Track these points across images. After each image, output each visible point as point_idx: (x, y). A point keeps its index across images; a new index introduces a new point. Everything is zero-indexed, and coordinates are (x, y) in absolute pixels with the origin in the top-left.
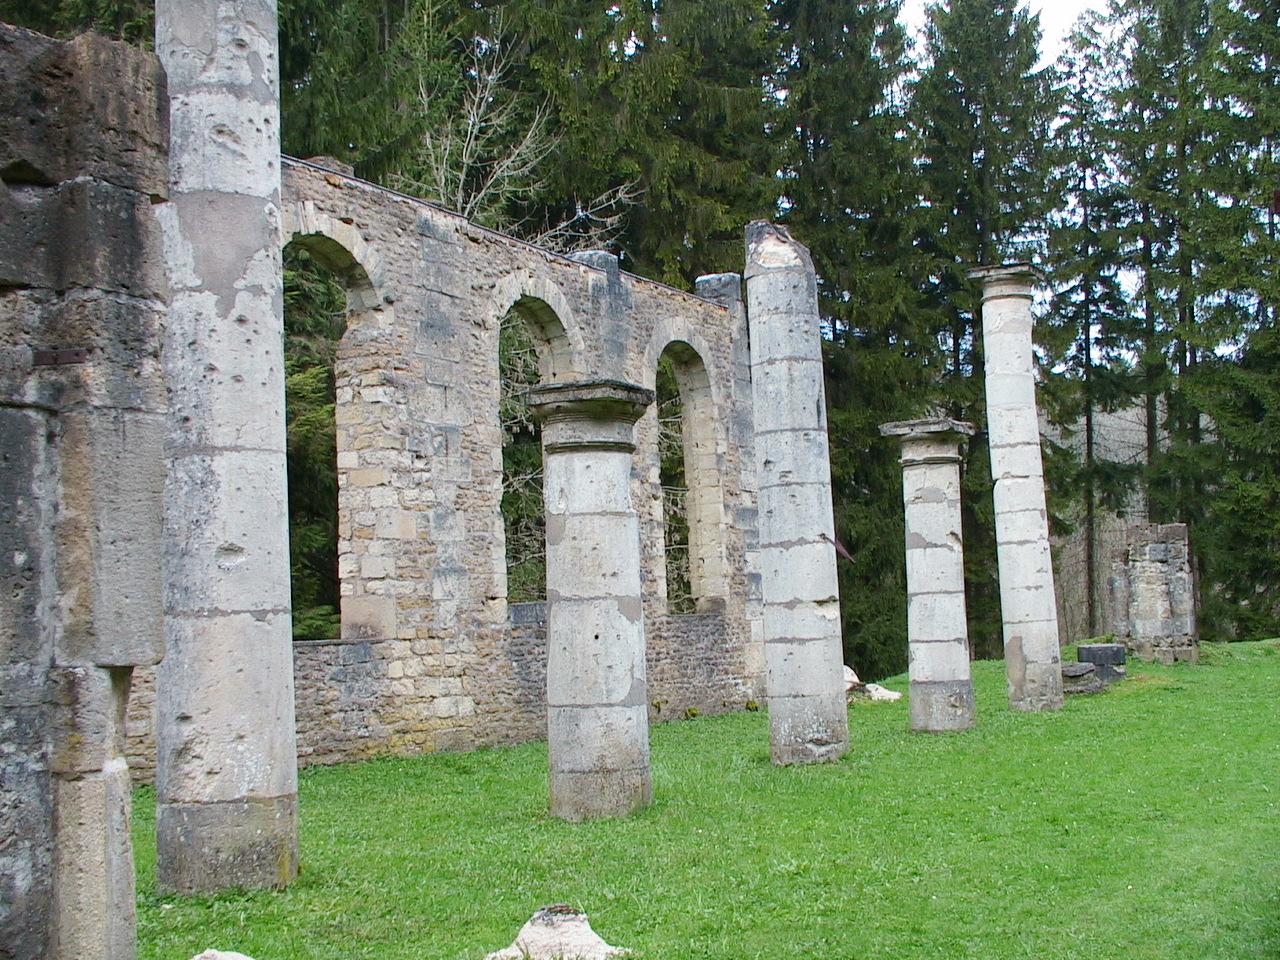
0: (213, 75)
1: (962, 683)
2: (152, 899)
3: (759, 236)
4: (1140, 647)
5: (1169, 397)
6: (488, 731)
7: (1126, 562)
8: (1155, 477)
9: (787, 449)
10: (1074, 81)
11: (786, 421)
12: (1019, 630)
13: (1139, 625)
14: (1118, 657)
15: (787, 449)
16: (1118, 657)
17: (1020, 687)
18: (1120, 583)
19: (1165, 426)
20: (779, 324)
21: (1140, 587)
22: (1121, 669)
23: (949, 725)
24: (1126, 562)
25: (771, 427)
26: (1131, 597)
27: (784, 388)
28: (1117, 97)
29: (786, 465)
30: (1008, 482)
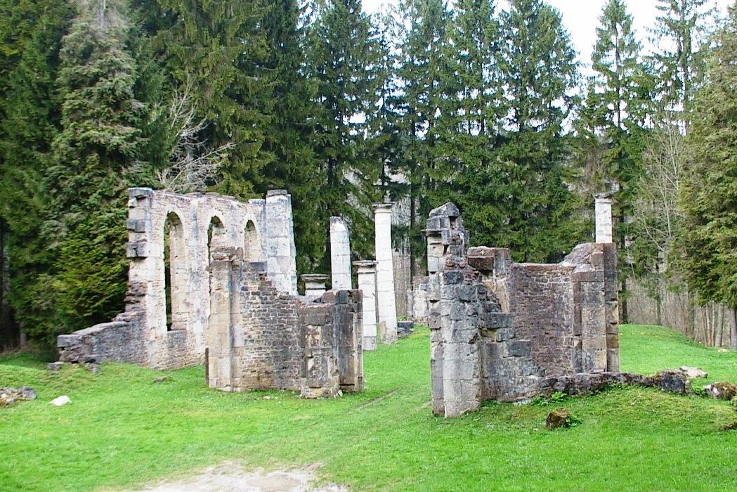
0: (282, 234)
1: (375, 337)
2: (610, 388)
3: (335, 221)
4: (416, 321)
5: (421, 199)
6: (719, 433)
7: (412, 290)
8: (415, 235)
9: (342, 279)
10: (380, 36)
11: (342, 271)
12: (384, 319)
13: (416, 312)
14: (411, 326)
15: (342, 279)
16: (411, 326)
17: (384, 337)
18: (410, 297)
19: (418, 211)
20: (340, 246)
21: (417, 299)
22: (412, 330)
23: (372, 349)
24: (412, 290)
25: (338, 272)
26: (414, 302)
27: (341, 262)
28: (397, 46)
29: (342, 283)
30: (382, 272)
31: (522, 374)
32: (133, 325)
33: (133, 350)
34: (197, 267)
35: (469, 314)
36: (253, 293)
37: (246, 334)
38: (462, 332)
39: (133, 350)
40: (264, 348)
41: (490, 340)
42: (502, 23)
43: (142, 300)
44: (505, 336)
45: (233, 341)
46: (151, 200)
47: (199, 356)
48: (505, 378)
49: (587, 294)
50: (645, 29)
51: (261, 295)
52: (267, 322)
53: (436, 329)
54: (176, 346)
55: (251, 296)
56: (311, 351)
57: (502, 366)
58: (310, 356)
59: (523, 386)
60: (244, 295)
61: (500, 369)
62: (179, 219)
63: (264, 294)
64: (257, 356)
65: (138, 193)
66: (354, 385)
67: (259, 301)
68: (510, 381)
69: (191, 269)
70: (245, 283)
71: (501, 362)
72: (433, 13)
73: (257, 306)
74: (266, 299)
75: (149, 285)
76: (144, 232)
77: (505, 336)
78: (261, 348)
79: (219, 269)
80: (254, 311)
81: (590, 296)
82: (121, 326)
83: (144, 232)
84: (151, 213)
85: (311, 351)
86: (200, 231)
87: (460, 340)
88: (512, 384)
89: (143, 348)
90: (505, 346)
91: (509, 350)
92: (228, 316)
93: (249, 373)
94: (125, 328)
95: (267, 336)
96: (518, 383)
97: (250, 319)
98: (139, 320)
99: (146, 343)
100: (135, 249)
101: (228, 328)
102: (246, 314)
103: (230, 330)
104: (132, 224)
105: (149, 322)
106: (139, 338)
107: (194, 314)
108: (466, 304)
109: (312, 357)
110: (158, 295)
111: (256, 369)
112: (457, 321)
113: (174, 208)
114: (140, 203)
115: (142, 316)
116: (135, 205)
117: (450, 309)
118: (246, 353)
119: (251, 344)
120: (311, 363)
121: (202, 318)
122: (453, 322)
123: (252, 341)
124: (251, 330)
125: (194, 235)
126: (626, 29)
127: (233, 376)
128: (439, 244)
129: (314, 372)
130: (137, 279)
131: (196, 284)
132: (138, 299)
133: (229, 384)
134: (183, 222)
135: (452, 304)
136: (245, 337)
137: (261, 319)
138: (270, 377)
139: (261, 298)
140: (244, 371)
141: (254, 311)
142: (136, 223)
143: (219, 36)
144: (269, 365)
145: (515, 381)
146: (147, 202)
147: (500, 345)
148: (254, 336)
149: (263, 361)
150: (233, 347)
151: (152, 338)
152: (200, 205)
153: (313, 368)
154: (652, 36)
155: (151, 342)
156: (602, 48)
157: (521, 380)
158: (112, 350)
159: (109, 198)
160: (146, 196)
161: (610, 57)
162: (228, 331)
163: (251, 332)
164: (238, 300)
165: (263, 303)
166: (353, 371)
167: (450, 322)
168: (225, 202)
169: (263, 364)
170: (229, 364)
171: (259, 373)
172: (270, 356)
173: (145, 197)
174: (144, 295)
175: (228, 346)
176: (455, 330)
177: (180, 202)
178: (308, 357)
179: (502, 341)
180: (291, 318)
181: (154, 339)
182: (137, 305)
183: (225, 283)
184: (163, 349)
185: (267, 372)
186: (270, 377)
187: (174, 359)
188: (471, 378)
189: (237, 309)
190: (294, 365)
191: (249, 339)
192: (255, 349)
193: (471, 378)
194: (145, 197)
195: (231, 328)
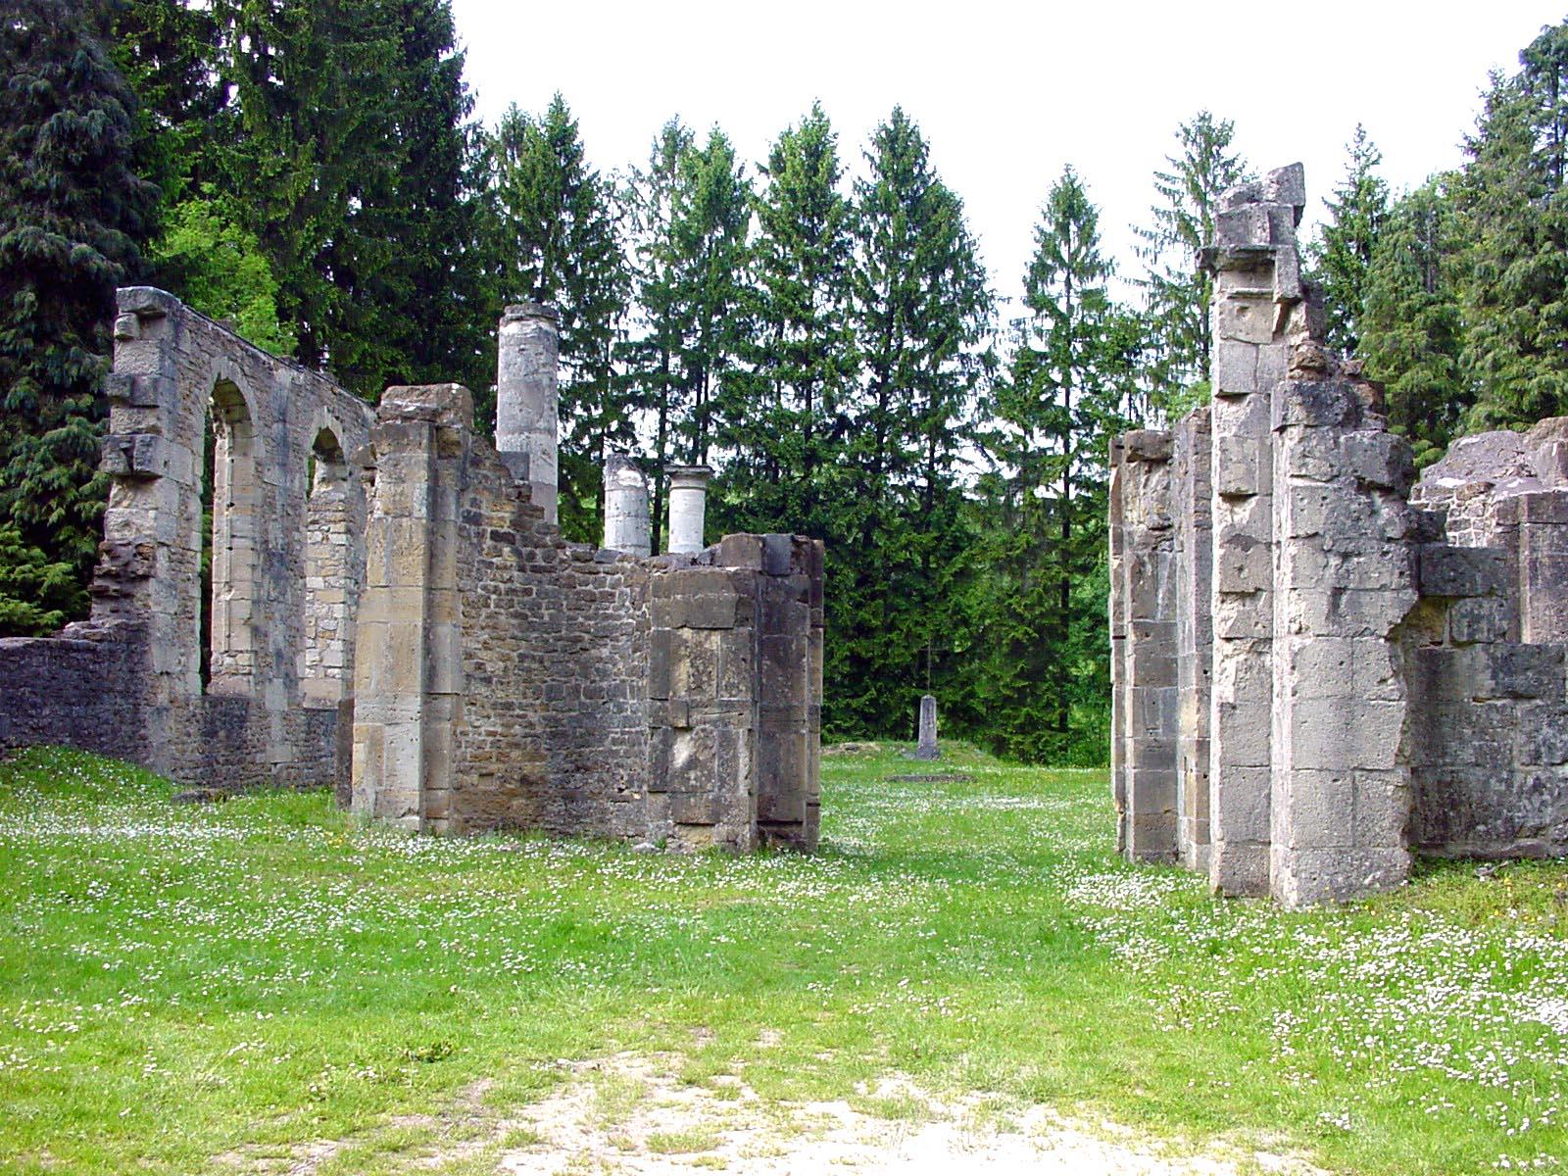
31: (1536, 758)
32: (112, 653)
33: (106, 722)
34: (280, 542)
35: (1391, 533)
36: (495, 536)
37: (469, 656)
38: (1365, 598)
39: (106, 722)
40: (521, 707)
41: (1426, 640)
42: (856, 204)
43: (139, 591)
44: (1484, 625)
45: (431, 675)
46: (177, 327)
47: (274, 771)
48: (1479, 771)
49: (1546, 560)
50: (1131, 229)
51: (518, 544)
52: (532, 627)
53: (1243, 596)
54: (222, 734)
55: (488, 543)
56: (689, 708)
57: (1468, 731)
58: (682, 723)
59: (1536, 800)
60: (469, 537)
61: (1462, 741)
62: (244, 404)
63: (526, 541)
64: (499, 730)
65: (144, 302)
66: (801, 823)
67: (512, 560)
68: (1493, 781)
69: (266, 542)
70: (474, 502)
71: (1466, 716)
72: (719, 182)
73: (506, 576)
74: (532, 556)
75: (162, 554)
76: (155, 407)
77: (1484, 625)
78: (509, 706)
79: (400, 448)
80: (496, 590)
81: (1555, 565)
82: (78, 650)
83: (155, 407)
84: (174, 362)
85: (689, 708)
86: (291, 454)
87: (1355, 627)
88: (1501, 795)
89: (138, 722)
90: (1483, 658)
91: (1494, 677)
92: (419, 596)
93: (475, 778)
94: (88, 656)
95: (529, 670)
96: (1521, 792)
97: (484, 612)
98: (129, 643)
99: (146, 712)
100: (125, 451)
101: (420, 631)
102: (472, 596)
103: (426, 637)
104: (118, 381)
105: (158, 657)
106: (126, 694)
107: (269, 660)
108: (1378, 500)
109: (688, 729)
110: (181, 586)
111: (493, 767)
112: (1346, 556)
113: (234, 373)
114: (147, 333)
115: (135, 636)
116: (135, 332)
117: (1325, 510)
118: (470, 716)
119: (483, 690)
120: (682, 751)
121: (287, 675)
122: (1334, 561)
123: (488, 681)
124: (486, 646)
125: (279, 459)
126: (1088, 237)
127: (427, 783)
128: (1260, 296)
129: (692, 775)
130: (130, 535)
131: (276, 583)
132: (127, 588)
133: (416, 807)
134: (254, 417)
135: (1332, 497)
136: (468, 666)
137: (516, 615)
138: (536, 794)
139: (517, 553)
140: (460, 771)
141: (496, 590)
142: (133, 381)
143: (312, 141)
144: (532, 759)
145: (1510, 785)
146: (165, 329)
147: (1463, 659)
148: (494, 667)
149: (517, 745)
150: (430, 694)
151: (162, 698)
152: (296, 388)
153: (692, 763)
154: (1144, 243)
155: (159, 711)
156: (1040, 272)
157: (1530, 781)
158: (46, 712)
159: (60, 391)
160: (166, 310)
161: (1055, 289)
162: (419, 640)
163: (484, 655)
164: (451, 550)
165: (522, 569)
166: (800, 783)
167: (1321, 559)
168: (350, 403)
169: (515, 754)
170: (417, 744)
171: (504, 780)
172: (539, 730)
173: (162, 316)
174: (145, 577)
175: (419, 689)
176: (1338, 592)
177: (248, 361)
178: (677, 729)
179: (1471, 643)
180: (607, 617)
181: (166, 703)
182: (125, 604)
183: (417, 491)
184: (189, 735)
185: (524, 780)
186: (536, 794)
187: (216, 766)
188: (1390, 765)
189: (448, 578)
190: (613, 761)
191: (478, 674)
192: (494, 706)
193: (1390, 765)
194: (162, 316)
195: (428, 630)
